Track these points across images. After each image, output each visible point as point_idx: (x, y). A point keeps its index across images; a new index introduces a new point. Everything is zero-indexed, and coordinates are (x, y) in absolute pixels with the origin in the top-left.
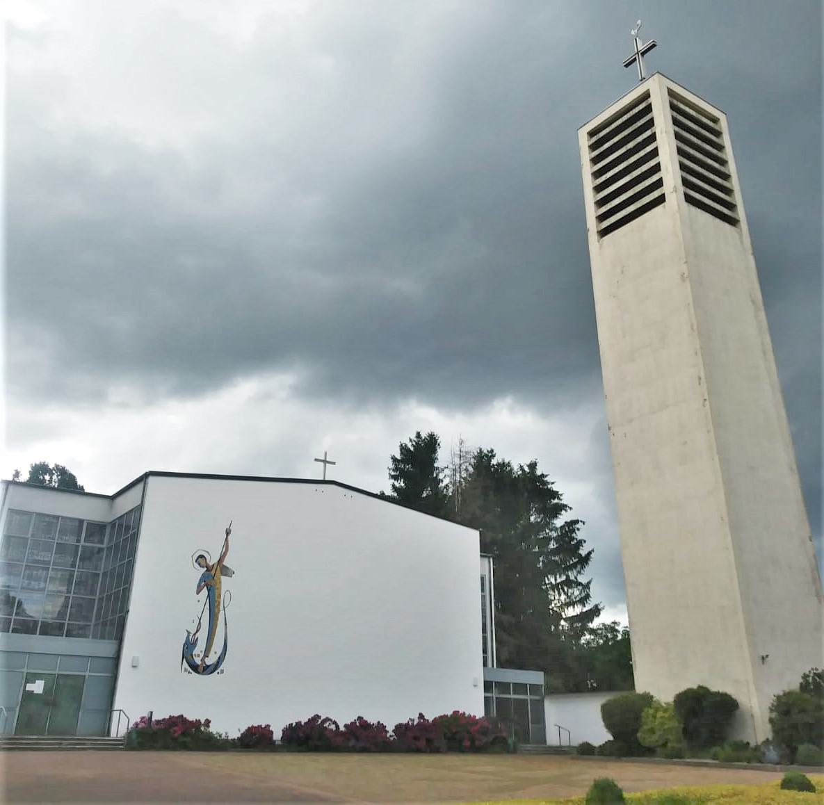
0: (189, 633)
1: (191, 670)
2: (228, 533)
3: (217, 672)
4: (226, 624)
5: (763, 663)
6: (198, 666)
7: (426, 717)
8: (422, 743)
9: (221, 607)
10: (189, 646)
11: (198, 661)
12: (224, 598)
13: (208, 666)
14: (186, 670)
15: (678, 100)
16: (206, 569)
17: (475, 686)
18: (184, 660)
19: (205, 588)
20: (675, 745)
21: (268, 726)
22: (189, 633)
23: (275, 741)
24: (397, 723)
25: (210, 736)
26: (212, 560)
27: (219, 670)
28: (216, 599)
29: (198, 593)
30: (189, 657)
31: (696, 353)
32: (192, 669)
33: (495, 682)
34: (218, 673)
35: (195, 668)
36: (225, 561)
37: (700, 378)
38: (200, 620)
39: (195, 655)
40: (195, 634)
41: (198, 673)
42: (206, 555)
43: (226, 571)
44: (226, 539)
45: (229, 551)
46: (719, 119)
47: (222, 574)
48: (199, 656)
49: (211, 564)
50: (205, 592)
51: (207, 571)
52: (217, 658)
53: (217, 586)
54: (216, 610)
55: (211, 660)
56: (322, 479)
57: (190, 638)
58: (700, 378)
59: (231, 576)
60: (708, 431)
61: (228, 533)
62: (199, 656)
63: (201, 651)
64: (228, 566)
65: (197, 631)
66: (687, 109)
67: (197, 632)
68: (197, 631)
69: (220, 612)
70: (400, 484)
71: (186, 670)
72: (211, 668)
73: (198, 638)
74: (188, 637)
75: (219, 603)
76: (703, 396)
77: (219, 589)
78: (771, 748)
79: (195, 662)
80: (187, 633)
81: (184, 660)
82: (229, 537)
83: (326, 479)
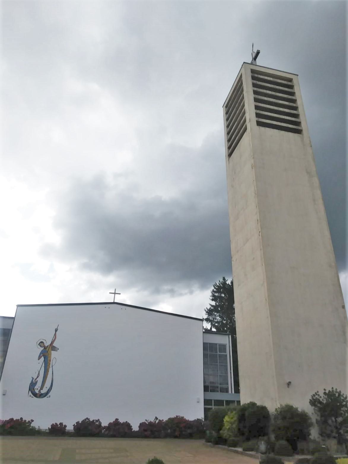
0: (33, 378)
1: (33, 396)
2: (56, 330)
3: (46, 397)
4: (53, 374)
5: (288, 387)
6: (37, 394)
7: (32, 423)
8: (148, 433)
9: (51, 366)
10: (32, 385)
11: (37, 391)
12: (53, 362)
13: (42, 394)
14: (30, 396)
15: (257, 74)
16: (43, 348)
17: (198, 402)
18: (30, 391)
19: (43, 357)
20: (234, 438)
21: (126, 422)
22: (33, 378)
23: (66, 429)
24: (110, 422)
25: (33, 429)
26: (47, 343)
27: (48, 396)
28: (48, 361)
29: (39, 359)
30: (33, 390)
31: (256, 207)
32: (34, 396)
33: (214, 400)
34: (47, 397)
35: (35, 395)
36: (54, 344)
37: (258, 220)
38: (39, 372)
39: (36, 389)
40: (36, 379)
41: (37, 397)
42: (44, 341)
43: (54, 348)
44: (55, 334)
45: (56, 340)
46: (292, 79)
47: (52, 350)
48: (37, 389)
49: (46, 345)
50: (42, 359)
51: (44, 349)
52: (47, 390)
53: (49, 356)
54: (48, 367)
55: (44, 391)
56: (113, 302)
57: (34, 381)
58: (258, 220)
59: (57, 351)
60: (261, 250)
61: (56, 330)
62: (37, 389)
63: (39, 387)
64: (55, 346)
65: (37, 377)
66: (266, 78)
67: (37, 378)
68: (37, 377)
69: (50, 368)
70: (213, 303)
71: (30, 396)
72: (44, 395)
73: (37, 381)
74: (32, 381)
75: (50, 364)
76: (259, 230)
77: (51, 357)
78: (263, 442)
79: (35, 392)
80: (32, 379)
81: (30, 391)
82: (57, 333)
83: (115, 301)
